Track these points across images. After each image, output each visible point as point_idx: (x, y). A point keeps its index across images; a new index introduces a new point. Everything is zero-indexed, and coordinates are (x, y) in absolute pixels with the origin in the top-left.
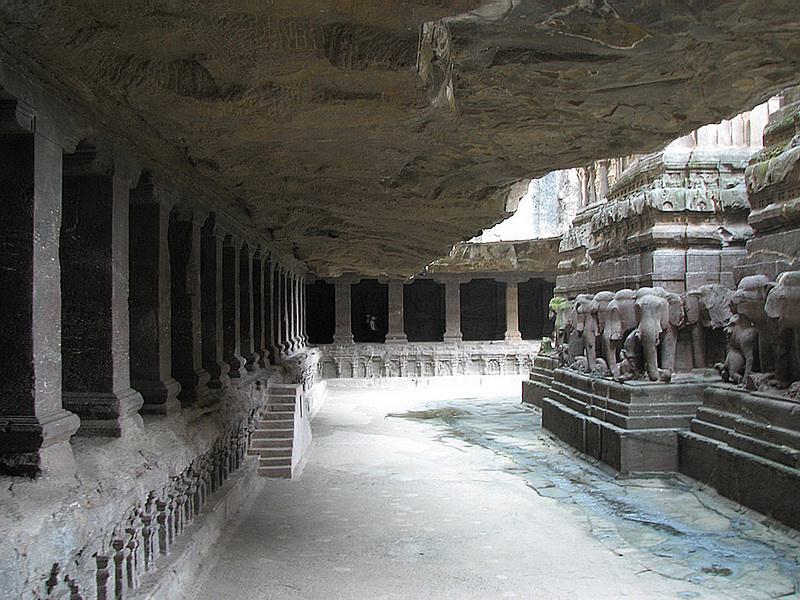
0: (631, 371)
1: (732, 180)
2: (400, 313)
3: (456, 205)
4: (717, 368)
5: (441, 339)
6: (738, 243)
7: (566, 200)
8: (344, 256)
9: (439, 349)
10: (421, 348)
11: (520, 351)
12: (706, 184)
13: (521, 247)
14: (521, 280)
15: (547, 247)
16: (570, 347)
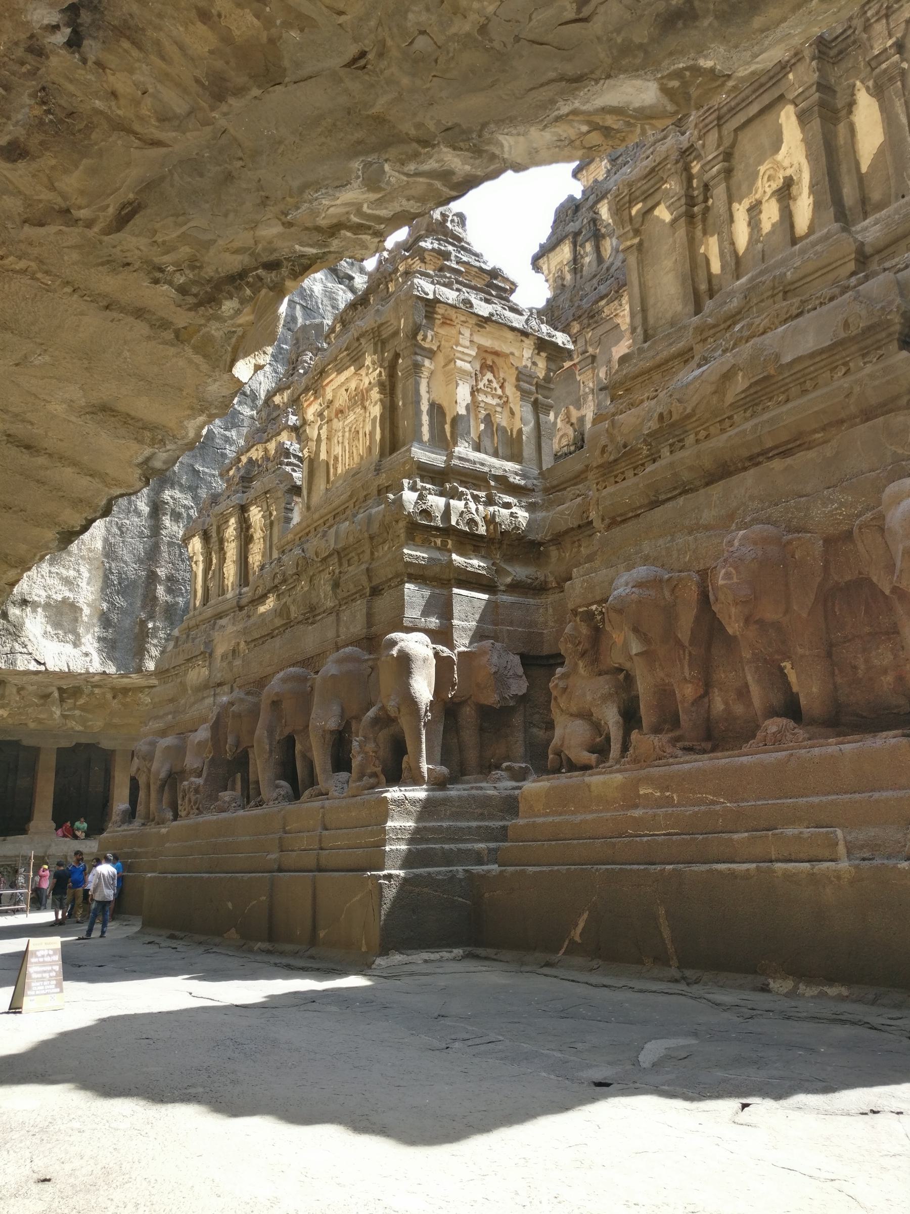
3: (139, 313)
4: (509, 769)
5: (23, 831)
12: (476, 498)
13: (69, 688)
14: (65, 743)
15: (109, 696)
16: (205, 784)
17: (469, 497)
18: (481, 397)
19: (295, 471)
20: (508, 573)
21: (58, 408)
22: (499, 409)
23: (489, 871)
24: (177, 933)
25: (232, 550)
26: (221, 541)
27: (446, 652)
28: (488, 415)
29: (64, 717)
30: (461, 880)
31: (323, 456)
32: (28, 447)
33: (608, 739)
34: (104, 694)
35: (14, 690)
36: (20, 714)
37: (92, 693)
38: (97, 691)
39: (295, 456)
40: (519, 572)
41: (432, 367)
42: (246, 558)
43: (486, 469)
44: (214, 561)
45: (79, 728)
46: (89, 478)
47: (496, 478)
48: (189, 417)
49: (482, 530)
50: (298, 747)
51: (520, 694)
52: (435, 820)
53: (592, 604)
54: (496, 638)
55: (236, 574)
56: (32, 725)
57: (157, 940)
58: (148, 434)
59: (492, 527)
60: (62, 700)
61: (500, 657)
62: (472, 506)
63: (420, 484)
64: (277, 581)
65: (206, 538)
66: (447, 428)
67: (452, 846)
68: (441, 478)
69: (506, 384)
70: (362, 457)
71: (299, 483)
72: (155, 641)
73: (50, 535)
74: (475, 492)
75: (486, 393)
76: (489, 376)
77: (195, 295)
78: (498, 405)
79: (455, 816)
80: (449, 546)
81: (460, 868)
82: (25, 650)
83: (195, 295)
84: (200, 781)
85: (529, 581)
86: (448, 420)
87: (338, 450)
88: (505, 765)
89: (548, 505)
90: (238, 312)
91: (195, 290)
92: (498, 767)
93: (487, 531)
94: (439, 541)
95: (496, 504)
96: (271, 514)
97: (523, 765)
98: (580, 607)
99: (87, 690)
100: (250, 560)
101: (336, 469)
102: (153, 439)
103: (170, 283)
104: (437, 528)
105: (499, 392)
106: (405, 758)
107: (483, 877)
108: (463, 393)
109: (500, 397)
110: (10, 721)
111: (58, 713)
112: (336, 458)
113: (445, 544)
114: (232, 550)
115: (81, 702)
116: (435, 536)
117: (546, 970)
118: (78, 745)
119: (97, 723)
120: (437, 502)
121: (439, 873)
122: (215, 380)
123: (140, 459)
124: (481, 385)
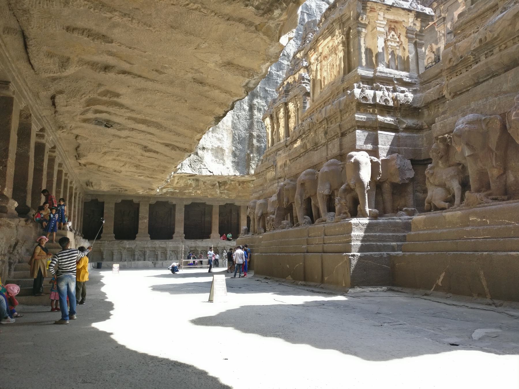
0: (345, 213)
1: (403, 89)
2: (146, 221)
5: (209, 238)
6: (408, 129)
7: (252, 155)
8: (114, 160)
9: (170, 244)
10: (158, 243)
11: (220, 245)
13: (222, 182)
14: (222, 204)
15: (237, 185)
17: (385, 89)
18: (389, 43)
19: (306, 86)
20: (404, 123)
21: (212, 65)
22: (398, 48)
23: (398, 254)
24: (268, 277)
25: (282, 122)
26: (278, 119)
27: (375, 159)
28: (393, 51)
29: (221, 193)
30: (385, 258)
31: (319, 77)
32: (201, 83)
33: (454, 196)
34: (235, 184)
35: (202, 183)
36: (205, 192)
37: (231, 183)
38: (232, 183)
39: (307, 79)
40: (409, 122)
41: (366, 32)
42: (288, 125)
43: (392, 76)
44: (275, 127)
45: (227, 197)
46: (225, 94)
47: (397, 80)
48: (263, 64)
49: (391, 104)
50: (312, 202)
51: (411, 177)
52: (373, 232)
53: (446, 134)
54: (399, 153)
55: (284, 132)
56: (209, 197)
57: (260, 279)
58: (247, 73)
59: (396, 102)
60: (220, 187)
61: (401, 161)
62: (386, 93)
63: (362, 85)
64: (301, 133)
65: (272, 118)
66: (374, 59)
67: (381, 243)
68: (370, 81)
69: (401, 36)
70: (335, 76)
71: (309, 91)
72: (254, 162)
73: (212, 119)
74: (388, 87)
75: (391, 41)
76: (393, 33)
77: (263, 9)
78: (397, 46)
79: (382, 231)
80: (376, 112)
81: (385, 253)
82: (205, 167)
83: (263, 9)
84: (274, 217)
85: (414, 126)
86: (374, 55)
87: (325, 74)
88: (404, 209)
89: (422, 90)
90: (281, 15)
91: (262, 7)
92: (401, 210)
93: (394, 104)
94: (371, 110)
95: (397, 91)
96: (297, 105)
97: (413, 209)
98: (439, 136)
99: (229, 183)
100: (290, 126)
101: (324, 82)
102: (249, 75)
103: (252, 5)
104: (370, 105)
105: (398, 40)
106: (359, 206)
107: (396, 257)
108: (381, 43)
109: (398, 42)
110: (201, 195)
111: (219, 192)
112: (324, 78)
113: (374, 111)
114: (282, 122)
115: (227, 187)
116: (370, 108)
117: (425, 297)
118: (227, 204)
119: (233, 195)
120: (370, 93)
121: (375, 255)
122: (273, 46)
123: (244, 84)
124: (389, 38)
